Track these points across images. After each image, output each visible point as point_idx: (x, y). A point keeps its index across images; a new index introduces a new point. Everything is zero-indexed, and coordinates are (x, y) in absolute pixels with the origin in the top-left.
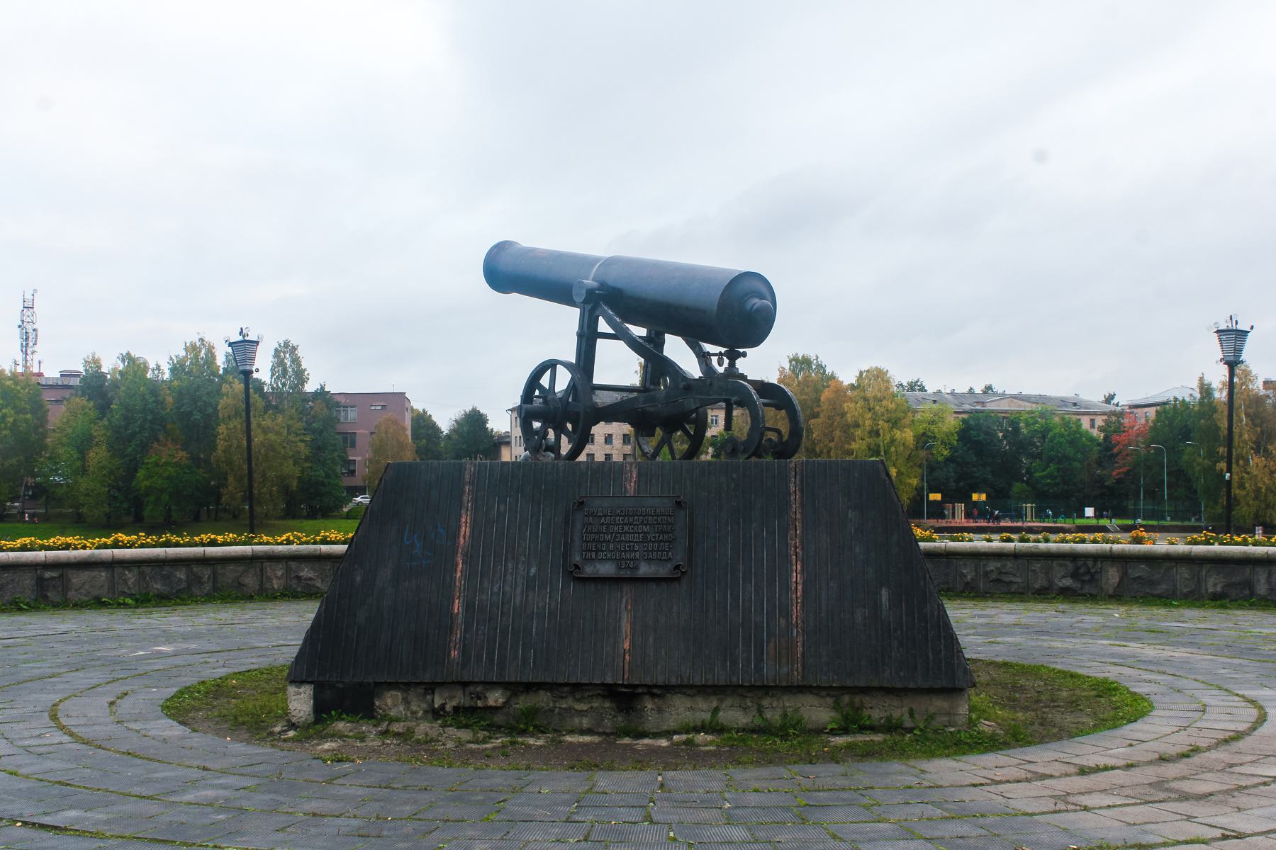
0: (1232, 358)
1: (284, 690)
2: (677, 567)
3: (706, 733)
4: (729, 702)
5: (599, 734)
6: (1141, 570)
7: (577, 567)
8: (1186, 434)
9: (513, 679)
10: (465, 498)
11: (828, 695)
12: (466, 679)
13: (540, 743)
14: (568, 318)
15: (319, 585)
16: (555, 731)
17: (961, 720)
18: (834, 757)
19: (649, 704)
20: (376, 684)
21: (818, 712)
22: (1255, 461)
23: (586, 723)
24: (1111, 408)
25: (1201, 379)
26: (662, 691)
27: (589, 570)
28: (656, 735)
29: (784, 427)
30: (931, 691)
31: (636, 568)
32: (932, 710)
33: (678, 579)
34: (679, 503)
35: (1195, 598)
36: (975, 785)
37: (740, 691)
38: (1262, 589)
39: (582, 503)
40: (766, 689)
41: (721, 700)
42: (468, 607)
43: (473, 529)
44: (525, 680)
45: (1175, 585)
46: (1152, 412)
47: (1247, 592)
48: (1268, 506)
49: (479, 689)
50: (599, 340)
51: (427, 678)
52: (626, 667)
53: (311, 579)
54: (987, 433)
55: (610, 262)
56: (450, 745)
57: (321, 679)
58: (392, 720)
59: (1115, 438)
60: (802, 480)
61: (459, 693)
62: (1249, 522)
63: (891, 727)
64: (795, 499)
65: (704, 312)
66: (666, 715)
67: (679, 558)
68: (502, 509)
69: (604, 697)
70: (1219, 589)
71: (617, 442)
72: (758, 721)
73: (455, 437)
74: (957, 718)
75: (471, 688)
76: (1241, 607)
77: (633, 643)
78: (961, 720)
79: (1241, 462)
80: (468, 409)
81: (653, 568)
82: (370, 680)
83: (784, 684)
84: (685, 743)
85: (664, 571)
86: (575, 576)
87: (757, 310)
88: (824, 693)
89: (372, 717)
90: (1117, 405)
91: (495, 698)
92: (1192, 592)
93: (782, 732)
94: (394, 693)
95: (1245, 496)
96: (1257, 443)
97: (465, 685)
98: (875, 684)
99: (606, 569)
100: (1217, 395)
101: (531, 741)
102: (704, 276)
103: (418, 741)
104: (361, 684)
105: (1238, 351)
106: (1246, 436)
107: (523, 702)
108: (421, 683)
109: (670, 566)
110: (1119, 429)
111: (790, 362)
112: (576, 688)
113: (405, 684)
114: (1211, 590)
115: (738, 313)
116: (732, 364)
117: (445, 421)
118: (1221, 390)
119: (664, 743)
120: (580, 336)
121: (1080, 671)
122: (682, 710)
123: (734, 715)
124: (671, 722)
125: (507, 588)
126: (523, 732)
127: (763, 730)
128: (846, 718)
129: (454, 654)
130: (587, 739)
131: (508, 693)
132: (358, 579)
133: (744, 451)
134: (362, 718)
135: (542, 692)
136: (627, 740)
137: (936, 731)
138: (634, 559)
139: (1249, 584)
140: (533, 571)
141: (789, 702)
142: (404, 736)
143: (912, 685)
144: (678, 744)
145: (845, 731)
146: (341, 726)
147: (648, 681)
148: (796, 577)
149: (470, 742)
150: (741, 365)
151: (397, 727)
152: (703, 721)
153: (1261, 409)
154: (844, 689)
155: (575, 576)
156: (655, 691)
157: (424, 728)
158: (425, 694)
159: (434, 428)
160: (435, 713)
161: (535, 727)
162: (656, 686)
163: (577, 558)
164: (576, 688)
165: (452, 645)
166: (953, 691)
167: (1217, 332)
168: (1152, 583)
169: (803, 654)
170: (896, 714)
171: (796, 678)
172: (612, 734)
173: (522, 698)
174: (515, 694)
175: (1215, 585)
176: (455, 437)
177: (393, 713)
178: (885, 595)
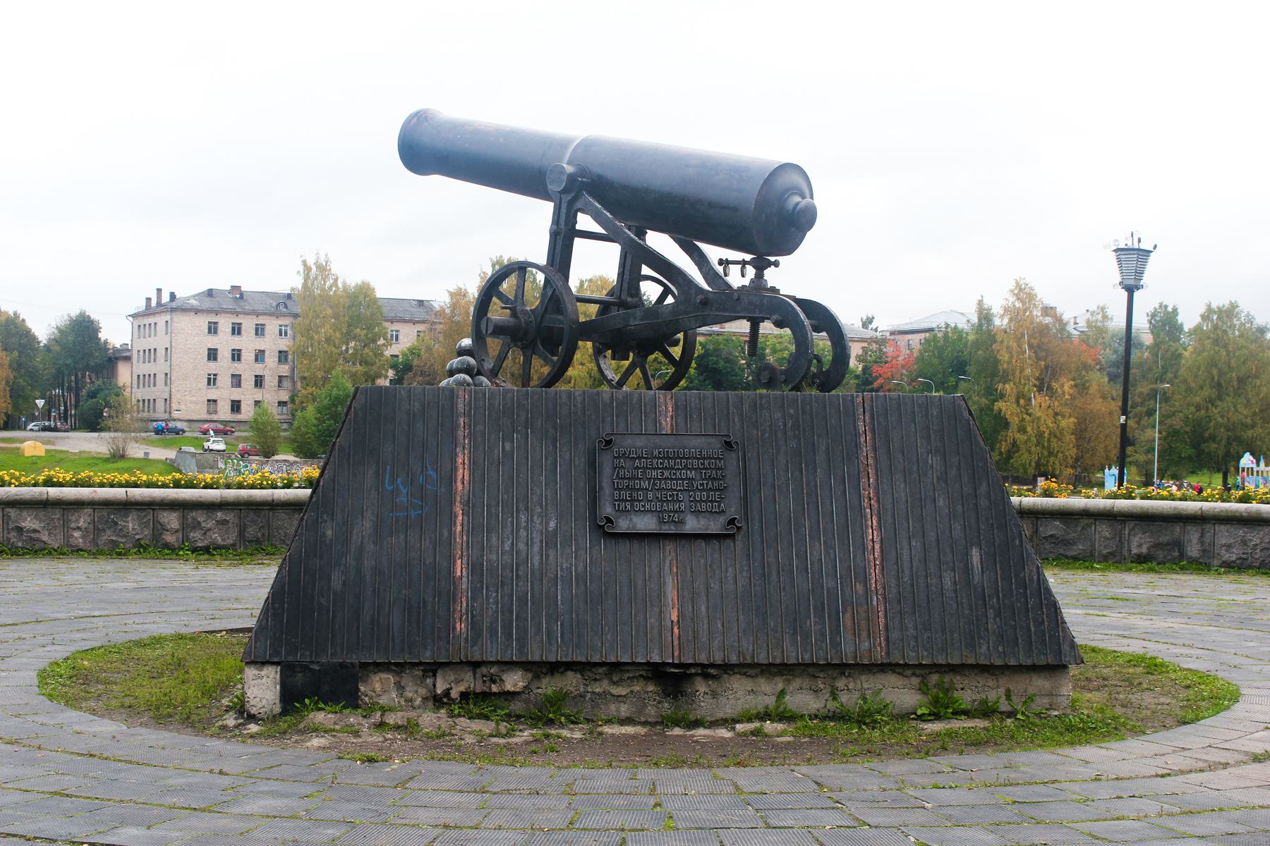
0: (1132, 282)
1: (241, 671)
2: (732, 521)
3: (772, 721)
4: (797, 683)
5: (644, 724)
6: (1054, 528)
7: (609, 520)
8: (959, 367)
9: (537, 658)
10: (460, 433)
11: (914, 674)
12: (477, 658)
13: (578, 735)
14: (541, 213)
15: (45, 538)
16: (588, 720)
17: (1064, 702)
18: (924, 750)
19: (701, 687)
20: (364, 666)
21: (902, 694)
22: (1038, 401)
23: (624, 710)
24: (868, 334)
25: (980, 303)
26: (715, 671)
27: (623, 525)
28: (714, 724)
29: (828, 357)
30: (1034, 669)
31: (682, 522)
32: (1031, 691)
33: (732, 536)
34: (728, 445)
35: (1117, 559)
36: (1162, 776)
37: (811, 670)
38: (1193, 550)
39: (609, 442)
40: (843, 669)
41: (788, 682)
42: (475, 569)
43: (472, 473)
44: (552, 659)
45: (1093, 546)
46: (916, 339)
47: (1176, 554)
48: (1051, 454)
49: (493, 670)
50: (576, 240)
51: (427, 657)
52: (676, 643)
53: (35, 531)
54: (727, 360)
55: (586, 145)
56: (470, 739)
57: (290, 658)
58: (384, 710)
59: (876, 369)
60: (872, 418)
61: (468, 676)
62: (1031, 471)
63: (986, 711)
64: (866, 443)
65: (735, 209)
66: (722, 700)
67: (733, 511)
68: (508, 446)
69: (646, 678)
70: (1144, 550)
71: (271, 359)
72: (832, 705)
73: (56, 348)
74: (1060, 699)
75: (484, 670)
76: (1172, 571)
77: (681, 615)
78: (1064, 702)
79: (1022, 402)
80: (74, 313)
81: (703, 522)
82: (354, 659)
83: (866, 662)
84: (753, 733)
85: (715, 526)
86: (604, 531)
87: (802, 211)
88: (909, 672)
89: (357, 707)
90: (876, 330)
91: (514, 681)
92: (1112, 554)
93: (865, 719)
94: (384, 676)
95: (1026, 442)
96: (1041, 380)
97: (475, 665)
98: (971, 661)
99: (645, 523)
100: (997, 322)
101: (565, 733)
102: (738, 171)
103: (428, 736)
104: (342, 665)
105: (1139, 274)
106: (1028, 371)
107: (548, 686)
108: (421, 663)
109: (722, 520)
110: (881, 359)
111: (493, 265)
112: (615, 669)
113: (396, 664)
114: (1135, 551)
115: (770, 217)
116: (759, 275)
117: (43, 327)
118: (1002, 317)
119: (724, 733)
120: (554, 235)
121: (1101, 645)
122: (741, 694)
123: (803, 699)
124: (728, 708)
125: (522, 546)
126: (550, 722)
127: (840, 717)
128: (936, 702)
129: (461, 627)
130: (629, 730)
131: (530, 675)
132: (329, 533)
133: (786, 382)
134: (345, 707)
135: (570, 674)
136: (677, 731)
137: (1038, 715)
138: (680, 511)
139: (1178, 545)
140: (552, 524)
141: (868, 683)
142: (408, 729)
143: (1012, 662)
144: (745, 734)
145: (937, 717)
146: (320, 717)
147: (703, 659)
148: (872, 535)
149: (491, 735)
150: (772, 277)
151: (391, 719)
152: (767, 707)
153: (1046, 340)
154: (935, 668)
155: (604, 531)
156: (712, 671)
157: (430, 720)
158: (424, 677)
159: (28, 336)
160: (439, 701)
161: (567, 716)
162: (712, 666)
163: (608, 510)
164: (615, 669)
165: (457, 615)
166: (1057, 668)
167: (1115, 251)
168: (1067, 543)
169: (886, 626)
170: (992, 696)
171: (880, 656)
172: (656, 723)
173: (545, 681)
174: (537, 677)
175: (1140, 546)
176: (56, 348)
177: (383, 701)
178: (975, 556)
